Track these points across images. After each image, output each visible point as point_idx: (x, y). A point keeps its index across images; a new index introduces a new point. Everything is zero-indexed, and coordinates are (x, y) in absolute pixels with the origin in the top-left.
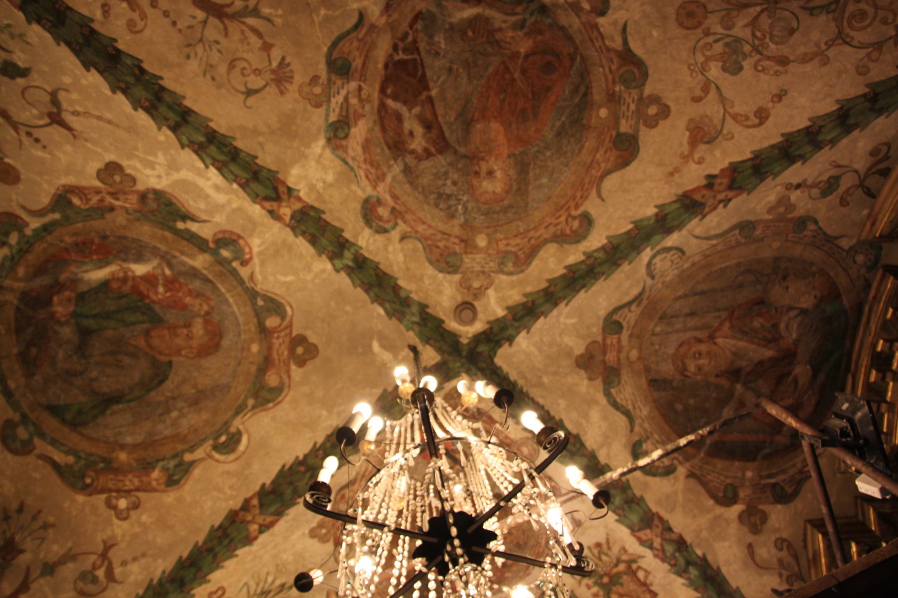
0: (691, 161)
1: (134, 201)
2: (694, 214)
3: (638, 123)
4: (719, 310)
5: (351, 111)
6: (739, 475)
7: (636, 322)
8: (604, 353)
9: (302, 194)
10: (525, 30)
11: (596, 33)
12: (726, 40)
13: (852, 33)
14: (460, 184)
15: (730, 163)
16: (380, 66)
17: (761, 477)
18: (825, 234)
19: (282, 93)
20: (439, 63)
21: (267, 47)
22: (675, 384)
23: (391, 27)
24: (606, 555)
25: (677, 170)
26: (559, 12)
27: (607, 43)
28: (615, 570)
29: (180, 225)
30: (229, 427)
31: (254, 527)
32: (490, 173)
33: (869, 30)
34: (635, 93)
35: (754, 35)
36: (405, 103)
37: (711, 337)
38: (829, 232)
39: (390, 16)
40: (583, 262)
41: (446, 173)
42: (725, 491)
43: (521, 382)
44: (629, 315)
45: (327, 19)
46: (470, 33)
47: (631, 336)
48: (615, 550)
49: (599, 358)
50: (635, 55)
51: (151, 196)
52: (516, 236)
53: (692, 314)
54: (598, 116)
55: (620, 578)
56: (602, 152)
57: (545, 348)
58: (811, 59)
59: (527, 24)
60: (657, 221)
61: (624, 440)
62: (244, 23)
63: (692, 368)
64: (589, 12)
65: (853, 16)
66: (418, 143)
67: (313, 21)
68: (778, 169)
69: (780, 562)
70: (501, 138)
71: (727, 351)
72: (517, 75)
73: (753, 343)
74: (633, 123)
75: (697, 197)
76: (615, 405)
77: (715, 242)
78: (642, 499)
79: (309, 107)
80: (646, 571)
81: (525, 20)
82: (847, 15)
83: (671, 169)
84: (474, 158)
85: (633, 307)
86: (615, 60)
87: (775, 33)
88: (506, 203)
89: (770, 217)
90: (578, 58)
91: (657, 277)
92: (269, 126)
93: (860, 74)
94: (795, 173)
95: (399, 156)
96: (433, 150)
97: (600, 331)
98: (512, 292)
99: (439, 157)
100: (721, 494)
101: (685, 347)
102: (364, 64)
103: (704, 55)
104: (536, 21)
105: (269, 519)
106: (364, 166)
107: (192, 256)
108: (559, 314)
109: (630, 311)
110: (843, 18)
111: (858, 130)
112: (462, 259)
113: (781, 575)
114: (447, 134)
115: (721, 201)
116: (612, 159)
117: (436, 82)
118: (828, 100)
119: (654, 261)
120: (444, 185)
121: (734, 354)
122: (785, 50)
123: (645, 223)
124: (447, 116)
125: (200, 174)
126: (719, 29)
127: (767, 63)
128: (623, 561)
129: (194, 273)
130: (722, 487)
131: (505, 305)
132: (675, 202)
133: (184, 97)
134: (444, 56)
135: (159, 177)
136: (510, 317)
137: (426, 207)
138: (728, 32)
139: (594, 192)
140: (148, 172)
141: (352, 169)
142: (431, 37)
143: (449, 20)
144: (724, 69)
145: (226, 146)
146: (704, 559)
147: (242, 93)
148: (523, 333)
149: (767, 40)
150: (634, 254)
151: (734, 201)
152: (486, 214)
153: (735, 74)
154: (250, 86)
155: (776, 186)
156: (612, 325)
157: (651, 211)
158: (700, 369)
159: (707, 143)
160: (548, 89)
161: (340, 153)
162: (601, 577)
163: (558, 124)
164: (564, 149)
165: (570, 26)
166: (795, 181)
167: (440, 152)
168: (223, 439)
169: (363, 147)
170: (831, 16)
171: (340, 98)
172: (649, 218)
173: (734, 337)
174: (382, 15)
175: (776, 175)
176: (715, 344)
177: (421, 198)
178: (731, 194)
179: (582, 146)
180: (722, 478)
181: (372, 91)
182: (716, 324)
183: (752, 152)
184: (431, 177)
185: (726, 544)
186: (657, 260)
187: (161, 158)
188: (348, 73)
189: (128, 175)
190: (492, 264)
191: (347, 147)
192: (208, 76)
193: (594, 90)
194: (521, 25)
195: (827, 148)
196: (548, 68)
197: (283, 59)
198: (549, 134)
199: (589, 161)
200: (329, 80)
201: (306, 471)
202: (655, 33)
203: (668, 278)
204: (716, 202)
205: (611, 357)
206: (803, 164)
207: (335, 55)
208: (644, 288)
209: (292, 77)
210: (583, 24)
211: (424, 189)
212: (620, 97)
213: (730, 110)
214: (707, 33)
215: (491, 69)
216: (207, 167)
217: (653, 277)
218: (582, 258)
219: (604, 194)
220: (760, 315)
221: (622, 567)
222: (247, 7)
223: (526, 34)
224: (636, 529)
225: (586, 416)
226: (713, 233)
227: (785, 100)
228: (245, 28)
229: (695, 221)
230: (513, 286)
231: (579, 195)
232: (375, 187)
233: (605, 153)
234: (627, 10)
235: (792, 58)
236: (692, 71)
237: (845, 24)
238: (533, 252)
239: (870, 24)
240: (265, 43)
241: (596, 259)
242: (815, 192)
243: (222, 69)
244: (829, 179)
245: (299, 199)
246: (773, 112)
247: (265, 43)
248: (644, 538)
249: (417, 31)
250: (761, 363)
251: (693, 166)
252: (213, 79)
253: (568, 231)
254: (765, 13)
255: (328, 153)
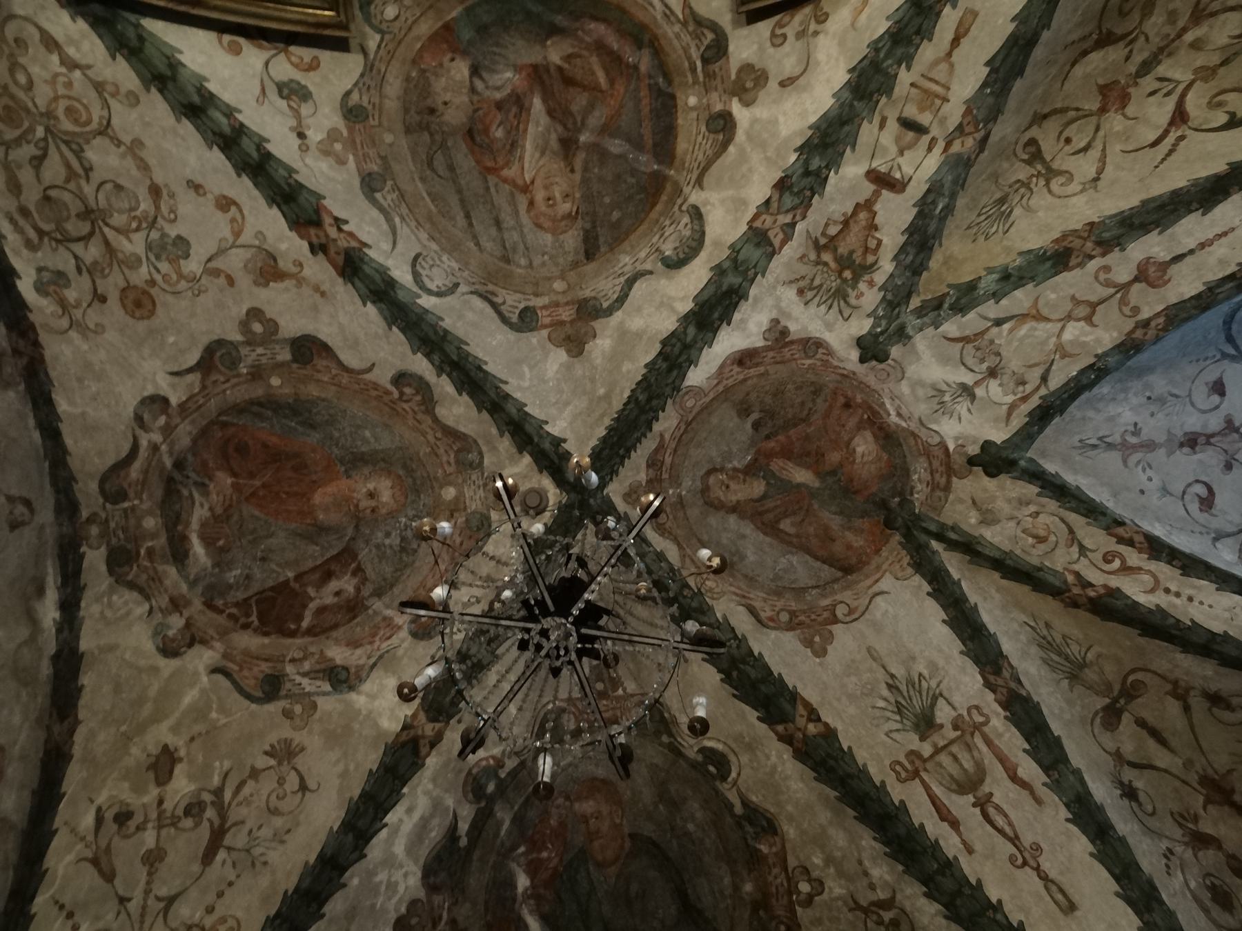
0: (303, 274)
1: (441, 898)
2: (362, 258)
3: (277, 342)
4: (488, 189)
5: (318, 667)
6: (694, 115)
7: (516, 291)
8: (562, 323)
9: (409, 713)
10: (207, 481)
11: (190, 404)
12: (152, 258)
13: (96, 119)
14: (388, 528)
15: (291, 229)
16: (266, 641)
17: (696, 82)
18: (362, 75)
19: (303, 749)
20: (257, 573)
21: (255, 774)
22: (588, 226)
23: (223, 634)
24: (812, 280)
25: (317, 289)
26: (177, 447)
27: (197, 390)
28: (833, 265)
29: (464, 842)
30: (697, 762)
31: (812, 728)
32: (371, 495)
33: (85, 101)
34: (244, 351)
35: (138, 229)
36: (305, 606)
37: (525, 189)
38: (360, 70)
39: (212, 638)
40: (449, 375)
41: (378, 547)
42: (716, 132)
43: (607, 422)
44: (509, 302)
45: (222, 710)
46: (221, 543)
47: (536, 295)
48: (804, 269)
49: (568, 330)
50: (202, 357)
51: (432, 880)
52: (437, 455)
53: (498, 223)
54: (280, 387)
55: (842, 256)
56: (319, 376)
57: (564, 396)
58: (142, 160)
59: (199, 480)
60: (381, 300)
61: (663, 282)
62: (230, 804)
63: (566, 207)
64: (168, 416)
65: (76, 121)
66: (347, 584)
67: (225, 725)
68: (282, 172)
69: (801, 35)
70: (331, 489)
71: (541, 163)
72: (257, 483)
73: (525, 130)
74: (277, 347)
75: (340, 260)
76: (621, 300)
77: (397, 220)
78: (732, 246)
79: (317, 716)
80: (827, 225)
81: (196, 483)
82: (77, 129)
83: (317, 296)
84: (357, 518)
85: (499, 300)
86: (213, 377)
87: (127, 206)
88: (401, 472)
89: (351, 157)
90: (224, 418)
91: (455, 280)
92: (338, 761)
93: (138, 102)
94: (283, 146)
95: (363, 604)
96: (353, 565)
97: (535, 333)
98: (501, 449)
99: (360, 557)
100: (721, 137)
101: (542, 220)
102: (266, 660)
103: (178, 281)
104: (194, 470)
105: (801, 710)
106: (377, 643)
107: (499, 824)
108: (520, 388)
109: (504, 303)
110: (82, 133)
111: (206, 84)
112: (473, 513)
113: (816, 33)
114: (334, 552)
115: (340, 230)
116: (325, 363)
117: (278, 573)
118: (182, 132)
119: (436, 289)
120: (391, 547)
121: (543, 153)
122: (143, 193)
123: (387, 313)
124: (315, 554)
125: (396, 831)
126: (144, 269)
127: (164, 209)
128: (819, 256)
129: (518, 820)
130: (712, 136)
131: (517, 455)
132: (353, 284)
133: (307, 863)
134: (250, 568)
135: (406, 875)
136: (529, 448)
137: (417, 564)
138: (144, 259)
139: (367, 376)
140: (401, 889)
141: (381, 657)
142: (230, 587)
143: (210, 569)
144: (187, 256)
145: (358, 808)
146: (800, 149)
147: (304, 795)
148: (548, 428)
149: (138, 213)
150: (429, 317)
151: (336, 213)
152: (417, 492)
153: (188, 243)
154: (296, 787)
155: (306, 165)
156: (525, 321)
157: (371, 309)
158: (567, 196)
159: (275, 260)
160: (265, 446)
161: (364, 675)
162: (845, 281)
163: (300, 429)
164: (326, 417)
165: (190, 433)
166: (295, 142)
167: (355, 556)
168: (712, 769)
169: (356, 647)
170: (85, 147)
171: (305, 682)
172: (381, 311)
173: (521, 158)
174: (212, 648)
175: (291, 171)
176: (532, 182)
177: (408, 572)
178: (328, 220)
179: (318, 398)
180: (700, 138)
181: (293, 646)
182: (507, 187)
183: (270, 207)
184: (384, 562)
185: (781, 119)
186: (432, 286)
187: (382, 877)
188: (277, 677)
189: (408, 910)
190: (474, 477)
191: (357, 666)
192: (286, 837)
193: (254, 395)
194: (202, 486)
195: (240, 117)
196: (242, 450)
197: (266, 753)
198: (314, 437)
199: (333, 388)
200: (287, 697)
201: (738, 669)
202: (171, 339)
203: (455, 265)
204: (342, 235)
205: (566, 314)
206: (268, 141)
207: (259, 694)
208: (472, 293)
209: (286, 740)
210: (183, 420)
211: (397, 570)
212: (253, 366)
213: (231, 240)
214: (152, 283)
215: (257, 513)
216: (386, 825)
217: (456, 285)
218: (444, 376)
219: (366, 365)
220: (486, 131)
221: (827, 257)
222: (213, 803)
223: (211, 479)
224: (771, 249)
225: (639, 335)
226: (385, 226)
227: (198, 179)
228: (234, 803)
229: (372, 253)
230: (494, 449)
231: (374, 393)
232: (400, 628)
233: (319, 371)
234: (155, 374)
235: (148, 182)
236: (200, 292)
237: (88, 129)
238: (452, 434)
239: (78, 100)
240: (250, 777)
241: (442, 362)
242: (305, 110)
243: (278, 822)
244: (282, 97)
245: (414, 716)
246: (217, 192)
247: (250, 777)
248: (781, 236)
249: (225, 604)
250: (550, 113)
251: (307, 272)
252: (289, 831)
253: (419, 398)
254: (108, 220)
255: (367, 687)
